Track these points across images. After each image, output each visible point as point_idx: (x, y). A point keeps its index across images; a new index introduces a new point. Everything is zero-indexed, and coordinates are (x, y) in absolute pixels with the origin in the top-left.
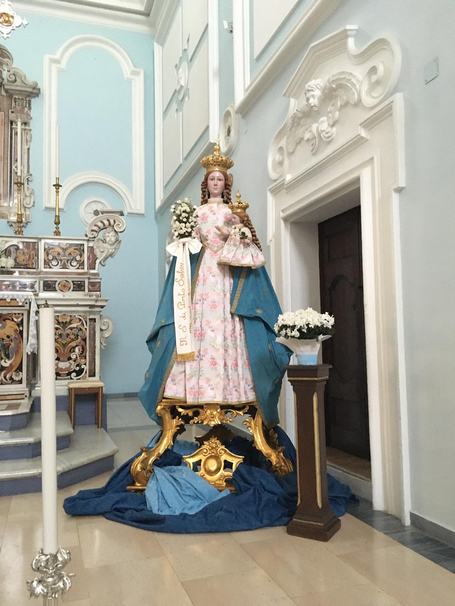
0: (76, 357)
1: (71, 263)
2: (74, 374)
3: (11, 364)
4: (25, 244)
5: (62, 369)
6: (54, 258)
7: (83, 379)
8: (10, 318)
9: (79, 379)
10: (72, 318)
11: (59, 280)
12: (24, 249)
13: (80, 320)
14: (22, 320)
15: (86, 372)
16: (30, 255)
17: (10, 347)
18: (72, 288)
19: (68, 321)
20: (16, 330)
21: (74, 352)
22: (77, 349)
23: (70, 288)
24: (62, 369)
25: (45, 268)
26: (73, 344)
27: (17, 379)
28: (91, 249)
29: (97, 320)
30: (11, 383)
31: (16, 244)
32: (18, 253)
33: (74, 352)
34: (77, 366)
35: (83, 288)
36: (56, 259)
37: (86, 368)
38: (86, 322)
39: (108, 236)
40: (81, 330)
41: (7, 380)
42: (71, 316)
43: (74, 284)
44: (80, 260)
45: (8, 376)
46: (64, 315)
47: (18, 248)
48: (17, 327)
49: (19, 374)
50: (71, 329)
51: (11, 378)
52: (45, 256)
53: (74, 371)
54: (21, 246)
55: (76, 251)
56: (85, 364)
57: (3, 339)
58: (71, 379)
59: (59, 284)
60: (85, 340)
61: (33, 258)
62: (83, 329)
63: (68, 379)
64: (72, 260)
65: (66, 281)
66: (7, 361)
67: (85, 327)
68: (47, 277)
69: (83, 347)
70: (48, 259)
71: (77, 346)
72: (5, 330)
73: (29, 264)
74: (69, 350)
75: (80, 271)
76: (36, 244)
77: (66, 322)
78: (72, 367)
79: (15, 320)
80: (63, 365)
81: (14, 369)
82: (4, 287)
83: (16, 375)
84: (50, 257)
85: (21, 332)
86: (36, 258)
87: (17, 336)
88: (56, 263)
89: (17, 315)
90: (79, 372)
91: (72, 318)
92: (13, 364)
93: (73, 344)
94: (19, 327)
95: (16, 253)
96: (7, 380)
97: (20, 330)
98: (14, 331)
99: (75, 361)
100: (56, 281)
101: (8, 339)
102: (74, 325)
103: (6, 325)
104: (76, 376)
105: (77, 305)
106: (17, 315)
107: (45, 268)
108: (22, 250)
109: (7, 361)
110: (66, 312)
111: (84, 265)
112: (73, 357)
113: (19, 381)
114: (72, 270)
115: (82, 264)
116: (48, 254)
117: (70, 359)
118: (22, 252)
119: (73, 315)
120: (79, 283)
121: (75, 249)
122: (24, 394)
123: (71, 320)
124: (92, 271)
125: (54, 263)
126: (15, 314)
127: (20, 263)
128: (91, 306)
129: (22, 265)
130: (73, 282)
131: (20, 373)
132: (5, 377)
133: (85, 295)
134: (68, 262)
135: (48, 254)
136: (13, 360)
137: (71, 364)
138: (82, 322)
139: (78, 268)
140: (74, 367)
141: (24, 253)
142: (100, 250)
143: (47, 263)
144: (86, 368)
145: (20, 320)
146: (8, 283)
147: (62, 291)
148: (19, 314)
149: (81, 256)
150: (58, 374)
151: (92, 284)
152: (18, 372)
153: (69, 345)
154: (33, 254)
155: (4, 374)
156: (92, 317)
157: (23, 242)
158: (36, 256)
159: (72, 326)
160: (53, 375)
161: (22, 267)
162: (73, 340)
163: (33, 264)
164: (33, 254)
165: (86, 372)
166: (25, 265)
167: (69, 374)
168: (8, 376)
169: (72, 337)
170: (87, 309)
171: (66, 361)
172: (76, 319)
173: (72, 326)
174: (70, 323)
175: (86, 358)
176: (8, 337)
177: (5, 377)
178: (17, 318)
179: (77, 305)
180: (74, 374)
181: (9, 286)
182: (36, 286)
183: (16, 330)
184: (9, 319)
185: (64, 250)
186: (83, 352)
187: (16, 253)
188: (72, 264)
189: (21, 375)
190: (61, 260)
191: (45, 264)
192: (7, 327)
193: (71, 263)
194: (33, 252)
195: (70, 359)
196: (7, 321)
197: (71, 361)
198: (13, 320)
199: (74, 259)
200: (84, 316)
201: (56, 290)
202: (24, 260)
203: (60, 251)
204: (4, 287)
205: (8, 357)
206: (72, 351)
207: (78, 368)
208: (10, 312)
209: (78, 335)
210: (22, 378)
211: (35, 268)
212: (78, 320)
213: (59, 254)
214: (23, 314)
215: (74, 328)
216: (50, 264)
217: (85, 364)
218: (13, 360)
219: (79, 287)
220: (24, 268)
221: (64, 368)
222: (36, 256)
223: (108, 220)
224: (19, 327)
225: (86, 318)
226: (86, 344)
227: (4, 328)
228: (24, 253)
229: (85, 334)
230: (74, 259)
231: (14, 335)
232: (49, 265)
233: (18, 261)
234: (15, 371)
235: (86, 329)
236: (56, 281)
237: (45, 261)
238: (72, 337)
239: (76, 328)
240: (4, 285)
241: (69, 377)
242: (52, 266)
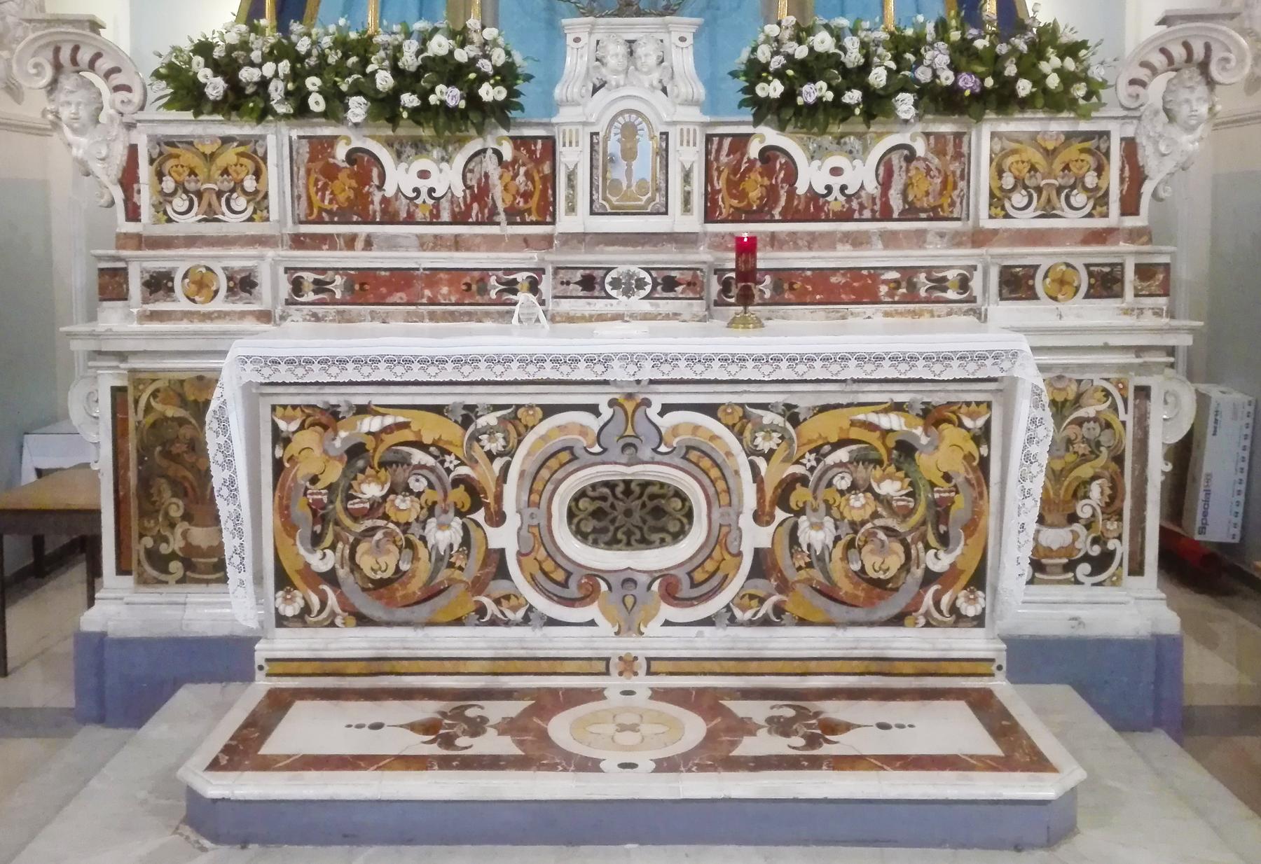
0: (1093, 516)
1: (1067, 198)
2: (1084, 568)
3: (953, 565)
4: (932, 139)
5: (1049, 552)
6: (1020, 183)
7: (1113, 584)
8: (954, 418)
9: (1100, 584)
10: (1083, 387)
11: (1045, 264)
12: (930, 156)
13: (1107, 394)
14: (988, 424)
15: (1121, 565)
16: (946, 177)
17: (953, 509)
18: (1084, 289)
19: (1071, 397)
20: (968, 457)
21: (1086, 497)
22: (1095, 490)
23: (1077, 289)
24: (1050, 549)
25: (991, 217)
26: (1086, 471)
27: (971, 611)
28: (1130, 146)
29: (1153, 394)
30: (955, 625)
31: (908, 142)
32: (912, 173)
33: (1086, 497)
34: (1095, 541)
35: (1116, 288)
36: (1026, 187)
37: (1122, 549)
38: (1125, 401)
39: (1188, 101)
40: (1108, 425)
41: (940, 612)
42: (1079, 381)
43: (1091, 275)
44: (1097, 188)
45: (945, 600)
46: (1060, 378)
47: (911, 157)
48: (971, 446)
49: (975, 599)
50: (1080, 422)
51: (954, 609)
52: (991, 178)
53: (1087, 558)
54: (920, 148)
55: (1084, 156)
56: (1119, 538)
57: (933, 485)
58: (1077, 582)
59: (1046, 276)
60: (1119, 459)
61: (955, 187)
62: (1117, 425)
63: (1067, 582)
64: (1073, 187)
65: (1068, 265)
66: (941, 554)
67: (1122, 416)
68: (1012, 256)
69: (1112, 480)
70: (1001, 188)
71: (1094, 478)
72: (938, 454)
73: (941, 206)
74: (1071, 492)
75: (1098, 223)
76: (965, 139)
77: (1066, 400)
78: (1078, 545)
79: (968, 422)
80: (1056, 537)
81: (964, 580)
82: (884, 289)
83: (968, 600)
84: (1008, 181)
85: (984, 463)
86: (962, 184)
87: (971, 476)
88: (1026, 200)
89: (973, 406)
90: (1101, 563)
91: (1083, 387)
92: (959, 566)
93: (1086, 471)
94: (978, 445)
95: (908, 171)
96: (940, 612)
97: (981, 457)
98: (965, 457)
99: (1088, 526)
100: (1036, 267)
101: (947, 486)
102: (1088, 411)
103: (941, 438)
104: (1091, 575)
105: (1106, 348)
106: (973, 406)
107: (991, 217)
108: (925, 159)
109: (941, 554)
110: (1066, 367)
111: (1107, 204)
112: (1084, 511)
113: (976, 618)
114: (1071, 221)
115: (1101, 199)
116: (1000, 173)
117: (1073, 518)
118: (921, 165)
119: (1086, 376)
120: (1107, 270)
121: (1082, 151)
122: (992, 660)
123: (1079, 396)
124: (1130, 222)
125: (1019, 199)
126: (968, 404)
127: (918, 205)
128: (1139, 350)
129: (924, 210)
130: (1087, 266)
131: (980, 593)
132: (937, 604)
133: (1127, 312)
134: (1059, 194)
135: (1000, 173)
136: (958, 551)
137: (1076, 536)
138: (1114, 399)
139: (1090, 215)
140: (1085, 545)
141: (928, 170)
142: (1157, 150)
143: (998, 200)
144: (1122, 549)
145: (980, 422)
146: (894, 275)
147: (1055, 299)
148: (978, 404)
149: (1100, 170)
150: (1037, 566)
151: (1144, 272)
152: (972, 592)
153: (1073, 474)
154: (954, 173)
155: (937, 591)
156: (1143, 381)
157: (927, 135)
158: (962, 177)
159: (1081, 413)
160: (1027, 570)
161: (923, 215)
162: (1084, 459)
163: (952, 204)
164: (954, 173)
165: (1121, 565)
166: (934, 209)
167: (1070, 566)
168: (945, 600)
169: (1082, 448)
170: (1130, 359)
171: (1063, 527)
172: (1096, 390)
173: (1081, 413)
174: (1077, 402)
175: (1120, 519)
176: (947, 477)
177: (937, 604)
178: (973, 416)
179: (1106, 348)
180: (1084, 568)
181: (897, 284)
182: (976, 284)
183: (968, 457)
184: (950, 421)
185: (1050, 154)
186: (1112, 498)
187: (908, 171)
188: (1072, 200)
189: (981, 600)
190: (1039, 190)
191: (990, 205)
192: (944, 447)
193: (1067, 198)
194: (955, 167)
195: (1073, 518)
196: (944, 426)
197: (1077, 527)
198: (961, 425)
199: (1079, 183)
200: (1119, 381)
201: (1034, 297)
202: (927, 194)
203: (1037, 158)
204: (884, 289)
205: (944, 540)
206: (1081, 493)
207: (1096, 551)
208: (953, 399)
209: (1098, 444)
210: (984, 609)
211: (958, 219)
212: (1100, 395)
213: (1033, 168)
214: (989, 405)
215: (1088, 420)
216: (1007, 205)
217: (1119, 538)
218: (958, 551)
219: (1105, 283)
220: (929, 219)
221: (1055, 547)
222: (962, 177)
223: (1186, 45)
224: (978, 445)
225: (1125, 388)
226: (1122, 473)
227: (937, 448)
228: (928, 170)
229: (1120, 441)
230: (1079, 183)
231: (962, 471)
232: (1003, 208)
233: (910, 198)
234: (965, 588)
235: (1124, 423)
236: (1036, 267)
237: (992, 195)
238: (1082, 448)
239: (1095, 420)
240: (886, 282)
241: (1070, 575)
242: (1011, 212)
